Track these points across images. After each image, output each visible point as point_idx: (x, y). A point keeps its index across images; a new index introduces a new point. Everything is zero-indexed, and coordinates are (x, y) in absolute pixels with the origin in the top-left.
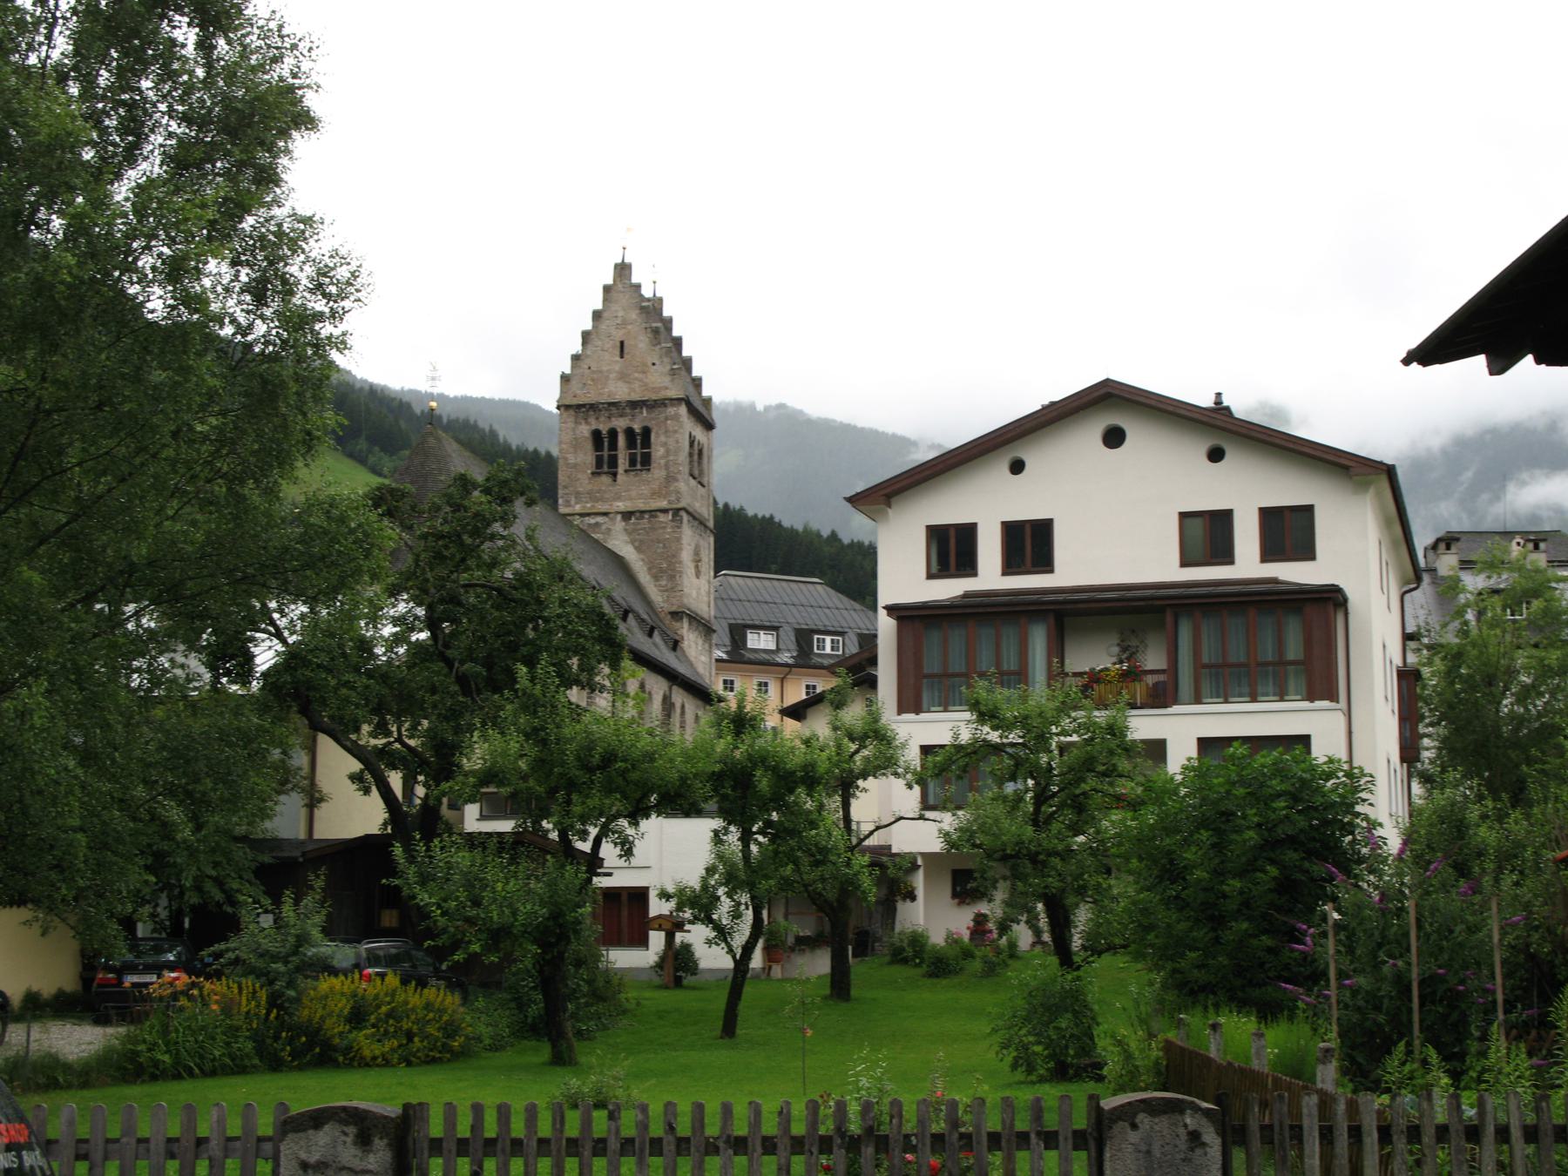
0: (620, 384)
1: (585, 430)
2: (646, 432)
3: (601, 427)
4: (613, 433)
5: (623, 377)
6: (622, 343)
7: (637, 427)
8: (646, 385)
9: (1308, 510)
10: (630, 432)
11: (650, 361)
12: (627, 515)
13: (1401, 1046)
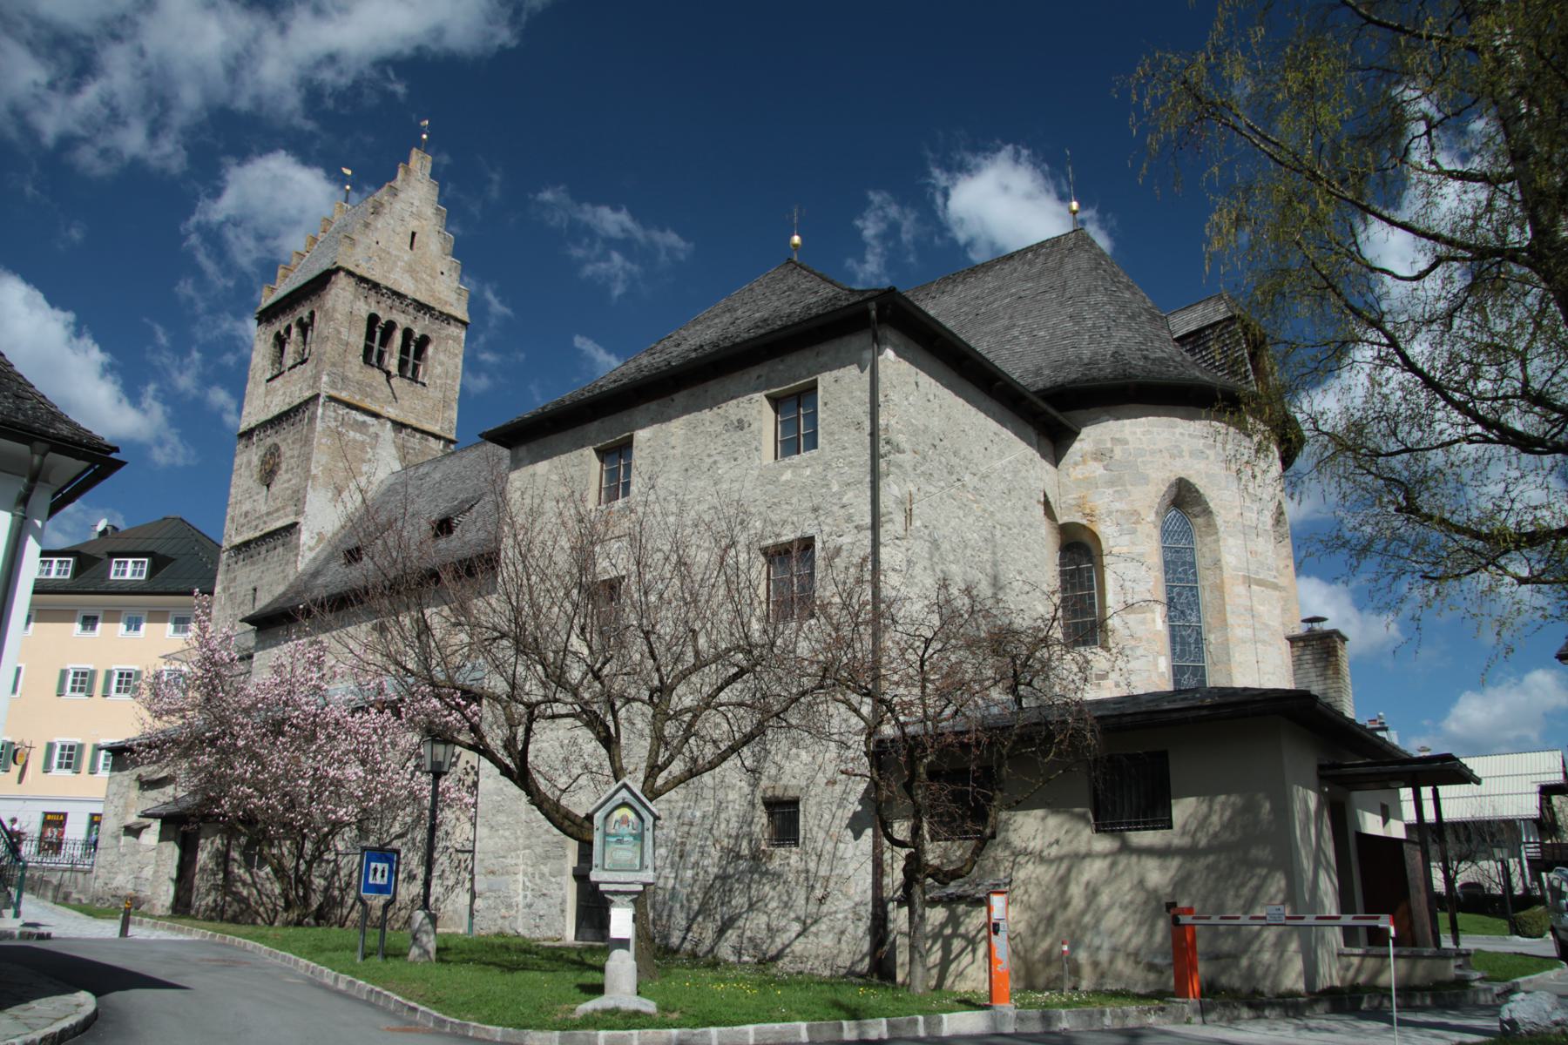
0: (407, 276)
1: (363, 309)
2: (424, 341)
3: (380, 314)
4: (391, 326)
5: (411, 270)
6: (414, 234)
7: (417, 333)
8: (432, 291)
9: (1170, 827)
10: (408, 333)
11: (439, 267)
12: (399, 426)
13: (1380, 734)
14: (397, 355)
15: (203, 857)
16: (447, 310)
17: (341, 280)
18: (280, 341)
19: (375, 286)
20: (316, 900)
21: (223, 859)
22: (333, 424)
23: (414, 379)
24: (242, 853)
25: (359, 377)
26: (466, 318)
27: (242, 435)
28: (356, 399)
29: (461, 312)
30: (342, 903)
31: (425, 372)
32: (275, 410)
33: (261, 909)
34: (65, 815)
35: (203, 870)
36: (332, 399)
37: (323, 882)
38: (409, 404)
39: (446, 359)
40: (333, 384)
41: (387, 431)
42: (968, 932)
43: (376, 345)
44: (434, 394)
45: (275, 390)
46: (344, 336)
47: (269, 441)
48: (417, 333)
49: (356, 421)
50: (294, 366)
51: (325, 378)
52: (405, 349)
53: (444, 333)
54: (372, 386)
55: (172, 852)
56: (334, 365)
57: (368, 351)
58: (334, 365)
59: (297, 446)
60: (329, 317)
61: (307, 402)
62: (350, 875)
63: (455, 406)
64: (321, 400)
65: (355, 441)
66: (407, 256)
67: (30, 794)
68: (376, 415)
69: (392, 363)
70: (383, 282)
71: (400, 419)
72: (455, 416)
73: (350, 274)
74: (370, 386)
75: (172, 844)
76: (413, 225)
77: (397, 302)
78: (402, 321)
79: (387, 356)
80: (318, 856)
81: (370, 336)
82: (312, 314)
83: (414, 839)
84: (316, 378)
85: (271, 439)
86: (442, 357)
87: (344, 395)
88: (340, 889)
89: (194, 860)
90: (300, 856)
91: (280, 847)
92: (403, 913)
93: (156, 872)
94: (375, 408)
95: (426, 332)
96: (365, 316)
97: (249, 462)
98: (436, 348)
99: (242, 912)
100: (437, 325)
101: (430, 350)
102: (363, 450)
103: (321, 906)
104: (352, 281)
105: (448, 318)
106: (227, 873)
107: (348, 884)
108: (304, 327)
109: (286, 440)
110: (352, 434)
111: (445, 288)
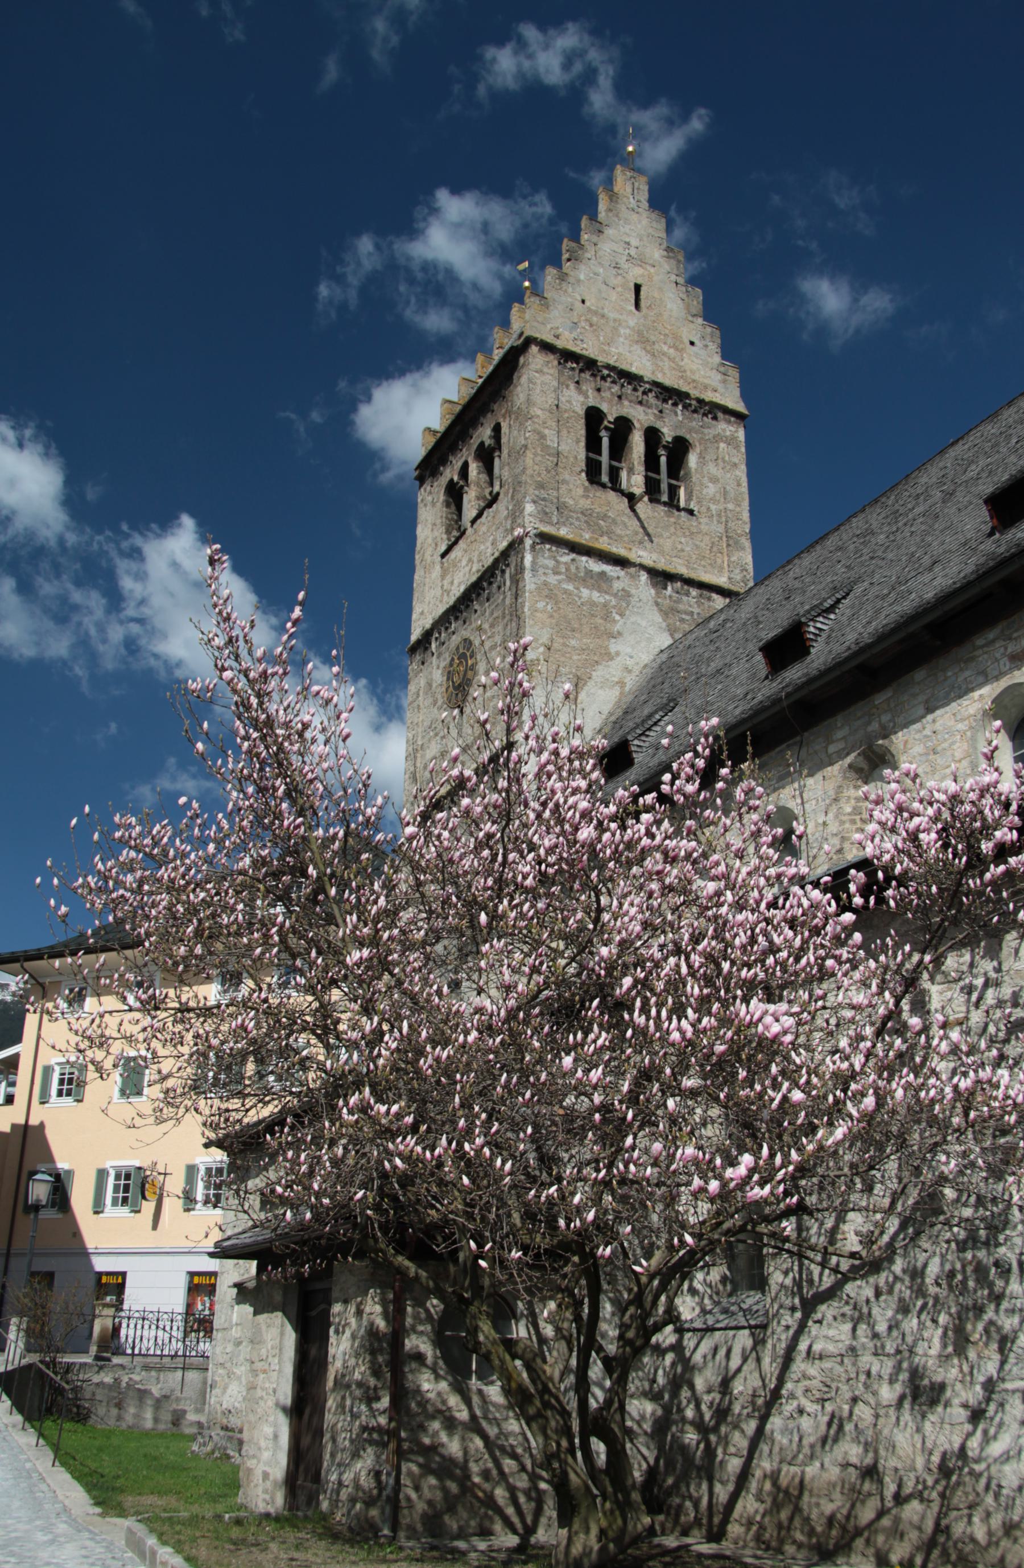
0: (637, 349)
1: (577, 401)
2: (680, 448)
3: (604, 407)
4: (624, 425)
5: (642, 340)
6: (638, 288)
7: (668, 434)
10: (652, 435)
12: (661, 577)
14: (640, 468)
15: (341, 1349)
16: (709, 396)
17: (535, 360)
18: (455, 494)
19: (589, 365)
20: (641, 1456)
21: (388, 1352)
22: (553, 579)
23: (673, 503)
24: (439, 1341)
25: (584, 503)
26: (740, 407)
27: (414, 649)
28: (585, 538)
29: (733, 400)
30: (708, 1470)
31: (689, 497)
32: (458, 590)
33: (500, 1494)
34: (124, 1274)
35: (341, 1384)
36: (545, 538)
37: (649, 1407)
38: (672, 544)
39: (720, 471)
40: (544, 516)
41: (643, 587)
42: (420, 1303)
43: (605, 458)
44: (708, 526)
45: (455, 564)
46: (552, 440)
47: (456, 640)
48: (668, 434)
49: (589, 572)
50: (479, 515)
51: (529, 508)
52: (651, 462)
53: (709, 433)
54: (609, 518)
55: (278, 1336)
56: (541, 486)
57: (592, 471)
58: (541, 486)
59: (500, 628)
60: (522, 417)
61: (505, 554)
62: (726, 1384)
63: (747, 544)
64: (528, 542)
65: (593, 604)
66: (633, 320)
67: (167, 1244)
68: (621, 562)
69: (635, 481)
70: (602, 359)
71: (662, 565)
72: (749, 559)
73: (547, 347)
74: (605, 517)
75: (278, 1317)
76: (636, 274)
77: (628, 389)
78: (641, 417)
79: (624, 475)
80: (638, 1342)
81: (593, 444)
82: (497, 429)
83: (916, 1274)
84: (516, 515)
85: (459, 633)
86: (712, 469)
87: (563, 532)
88: (699, 1425)
89: (323, 1362)
90: (588, 1342)
91: (533, 1319)
92: (913, 1510)
93: (252, 1388)
94: (618, 550)
95: (681, 433)
96: (582, 412)
97: (429, 685)
98: (701, 456)
99: (451, 1504)
100: (697, 421)
101: (693, 460)
102: (607, 617)
103: (652, 1473)
104: (552, 359)
105: (713, 410)
106: (402, 1395)
107: (722, 1413)
108: (487, 456)
109: (482, 627)
110: (585, 592)
111: (701, 366)
